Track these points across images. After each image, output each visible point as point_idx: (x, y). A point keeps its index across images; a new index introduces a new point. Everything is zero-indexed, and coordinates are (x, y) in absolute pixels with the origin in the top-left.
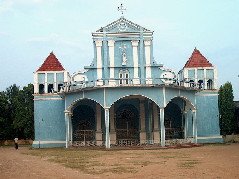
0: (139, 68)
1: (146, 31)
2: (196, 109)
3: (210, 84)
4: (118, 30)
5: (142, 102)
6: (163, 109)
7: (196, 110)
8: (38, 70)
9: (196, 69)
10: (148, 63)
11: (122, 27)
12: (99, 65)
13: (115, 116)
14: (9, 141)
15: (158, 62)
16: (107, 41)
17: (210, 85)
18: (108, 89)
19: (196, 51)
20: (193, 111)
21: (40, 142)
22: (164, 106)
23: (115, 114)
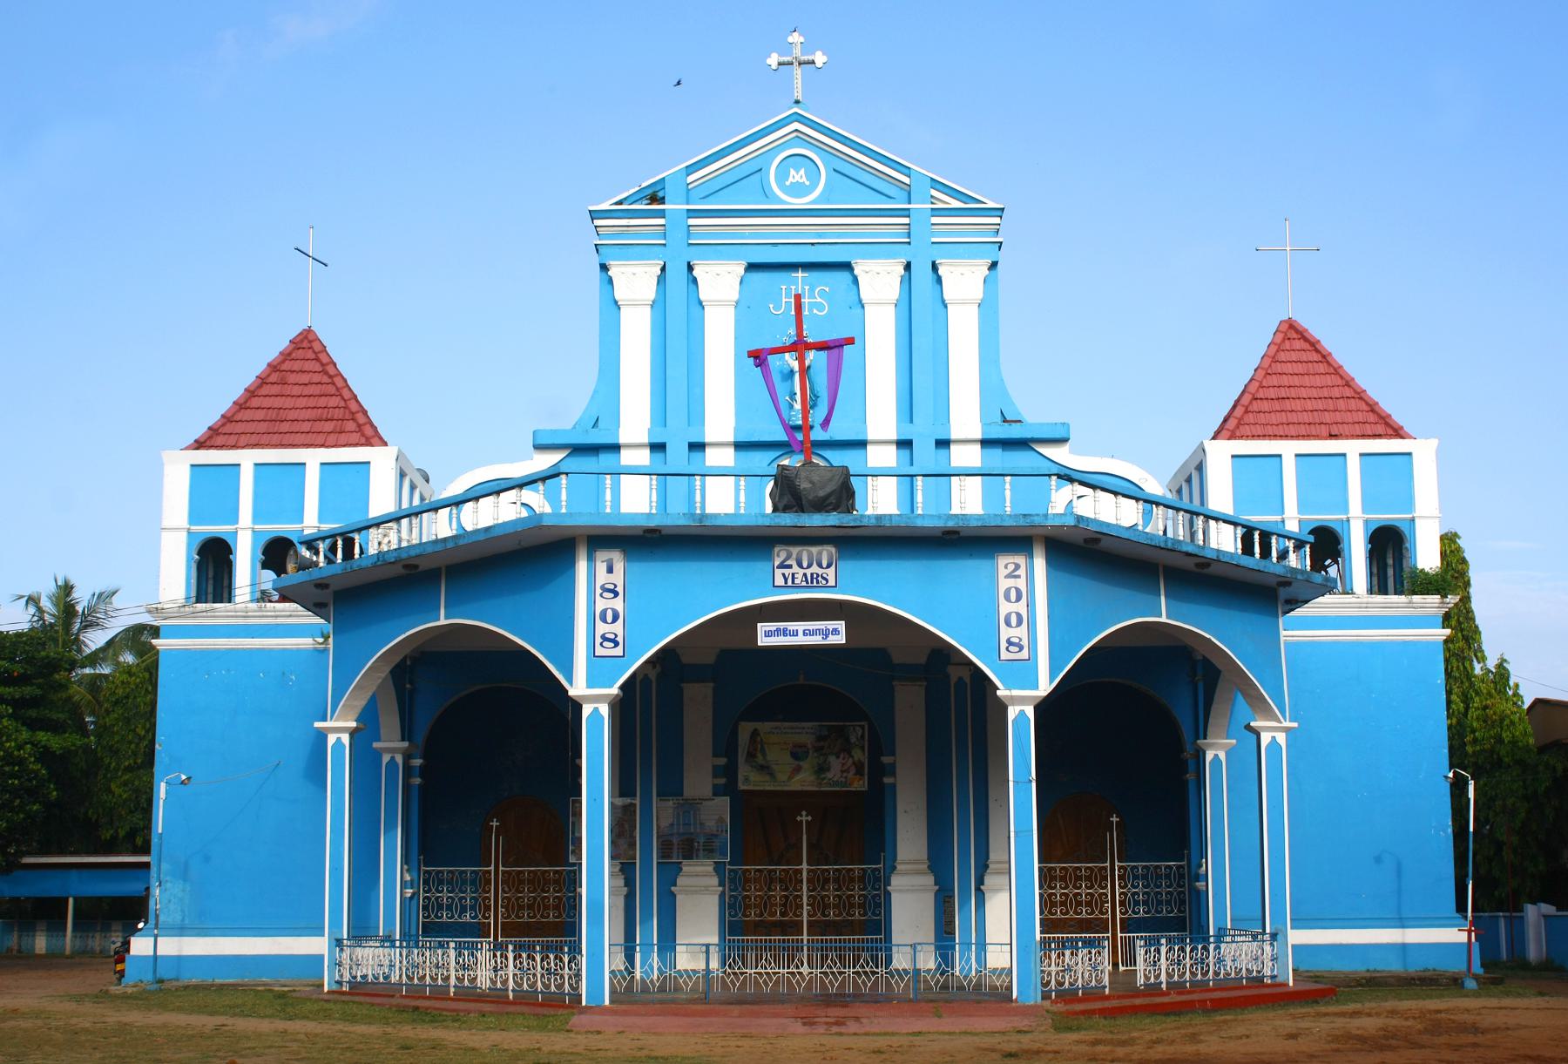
0: (905, 453)
1: (956, 204)
2: (1287, 724)
3: (1390, 561)
4: (766, 194)
5: (910, 672)
6: (1030, 711)
7: (1287, 730)
8: (200, 445)
9: (1289, 449)
10: (966, 420)
11: (797, 176)
12: (634, 425)
13: (715, 768)
14: (1426, 990)
15: (1035, 416)
16: (690, 268)
17: (1390, 572)
18: (605, 539)
19: (1291, 332)
20: (1266, 738)
21: (159, 939)
22: (1036, 687)
23: (715, 755)
